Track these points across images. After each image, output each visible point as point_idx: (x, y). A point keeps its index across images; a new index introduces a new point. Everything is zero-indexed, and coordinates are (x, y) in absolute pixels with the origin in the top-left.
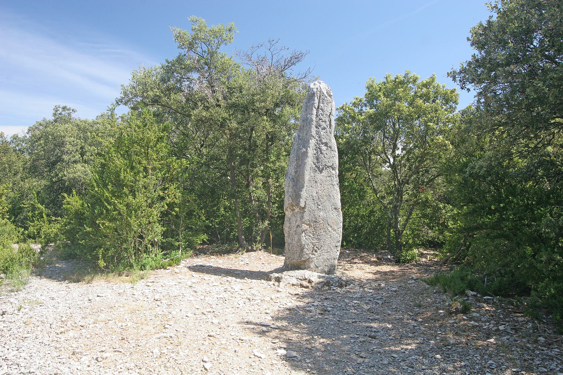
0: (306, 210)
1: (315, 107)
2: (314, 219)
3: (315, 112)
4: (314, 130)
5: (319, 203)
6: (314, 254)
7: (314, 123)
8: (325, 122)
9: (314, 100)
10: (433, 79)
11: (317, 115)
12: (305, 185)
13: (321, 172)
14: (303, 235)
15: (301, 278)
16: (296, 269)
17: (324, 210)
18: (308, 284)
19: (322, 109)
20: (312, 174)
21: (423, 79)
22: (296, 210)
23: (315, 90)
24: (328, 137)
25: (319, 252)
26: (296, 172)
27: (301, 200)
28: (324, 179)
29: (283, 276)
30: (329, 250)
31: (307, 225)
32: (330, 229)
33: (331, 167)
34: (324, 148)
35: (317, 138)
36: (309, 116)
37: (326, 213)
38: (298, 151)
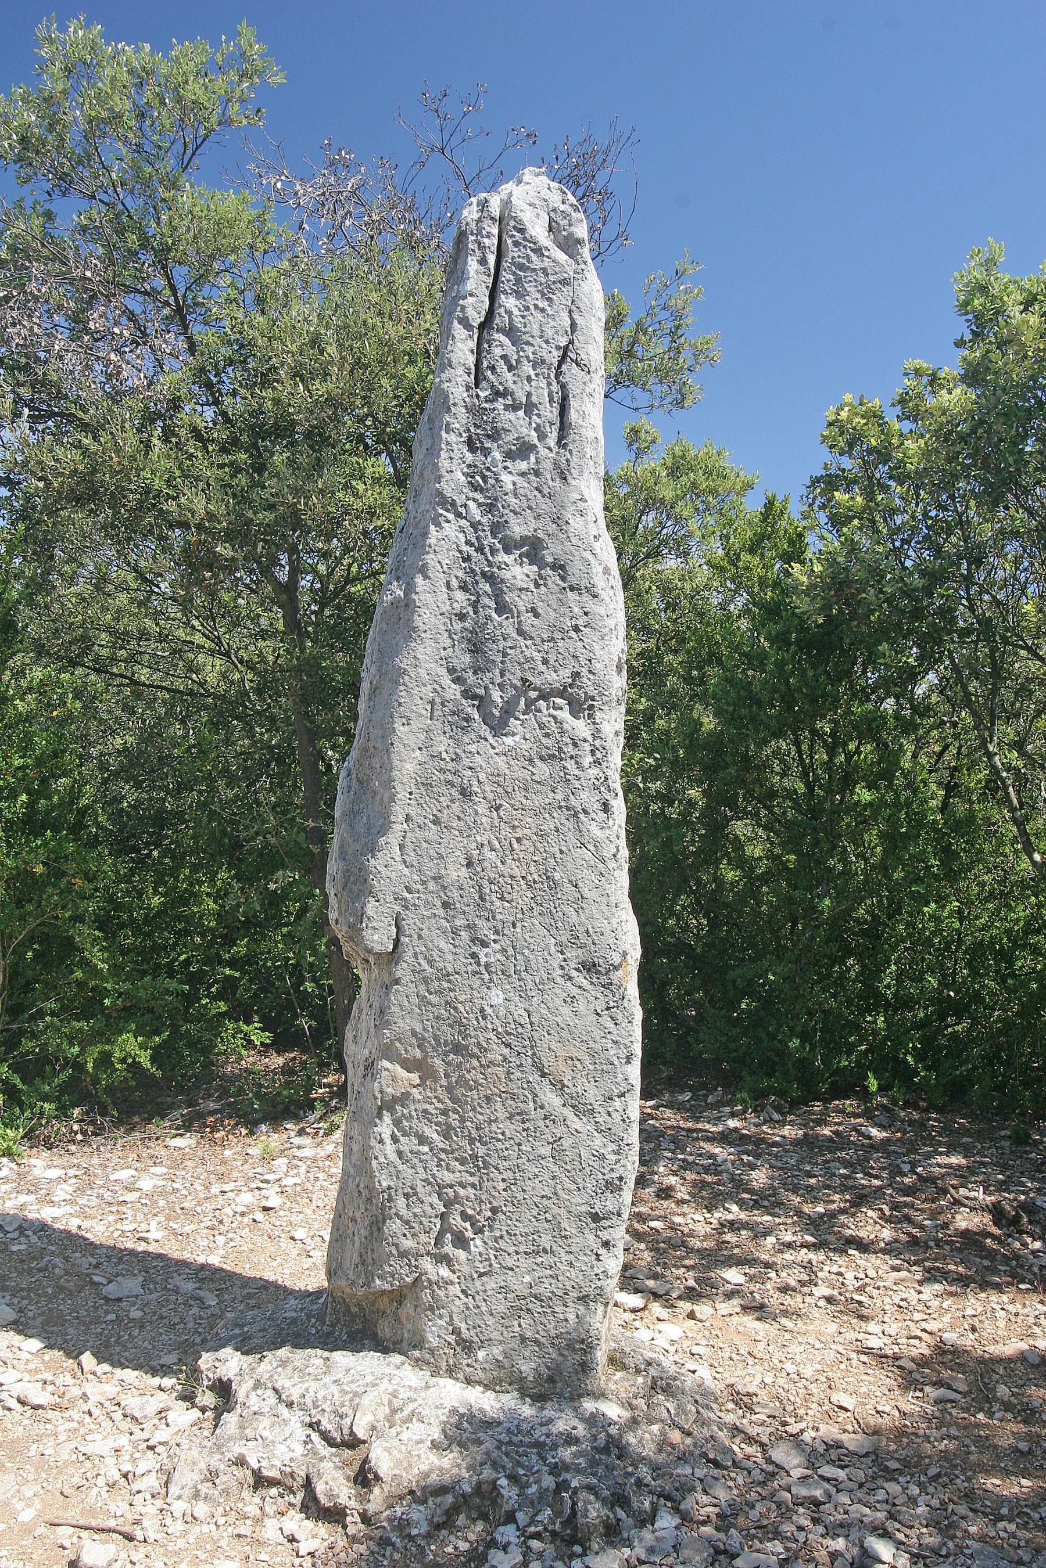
0: (402, 971)
2: (447, 1034)
3: (462, 348)
4: (453, 467)
5: (485, 929)
7: (459, 419)
8: (530, 408)
13: (499, 727)
14: (385, 1128)
16: (329, 1343)
17: (513, 971)
19: (511, 332)
20: (442, 745)
25: (477, 1244)
30: (545, 1241)
31: (409, 1066)
32: (552, 1099)
33: (562, 693)
34: (517, 572)
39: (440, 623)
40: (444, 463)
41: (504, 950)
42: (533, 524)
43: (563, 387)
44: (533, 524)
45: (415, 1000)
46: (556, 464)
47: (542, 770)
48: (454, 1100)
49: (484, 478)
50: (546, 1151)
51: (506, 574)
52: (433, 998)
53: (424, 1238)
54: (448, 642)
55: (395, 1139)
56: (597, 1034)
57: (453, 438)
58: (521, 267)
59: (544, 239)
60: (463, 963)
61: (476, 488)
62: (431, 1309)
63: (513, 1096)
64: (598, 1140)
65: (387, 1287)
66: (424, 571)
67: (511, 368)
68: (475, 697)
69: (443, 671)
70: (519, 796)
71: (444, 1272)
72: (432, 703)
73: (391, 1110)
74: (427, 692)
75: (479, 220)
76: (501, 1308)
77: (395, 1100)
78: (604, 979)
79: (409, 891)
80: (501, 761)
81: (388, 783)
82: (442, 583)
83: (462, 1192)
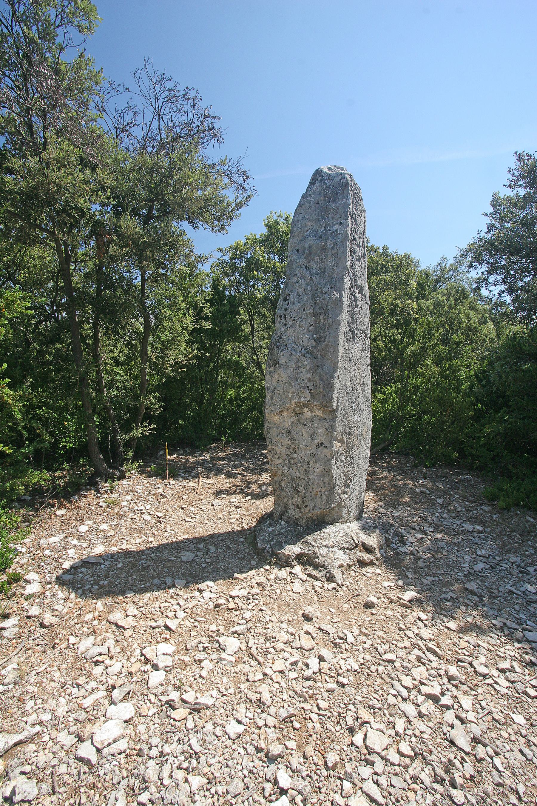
2: (347, 430)
12: (340, 364)
26: (318, 341)
60: (350, 409)
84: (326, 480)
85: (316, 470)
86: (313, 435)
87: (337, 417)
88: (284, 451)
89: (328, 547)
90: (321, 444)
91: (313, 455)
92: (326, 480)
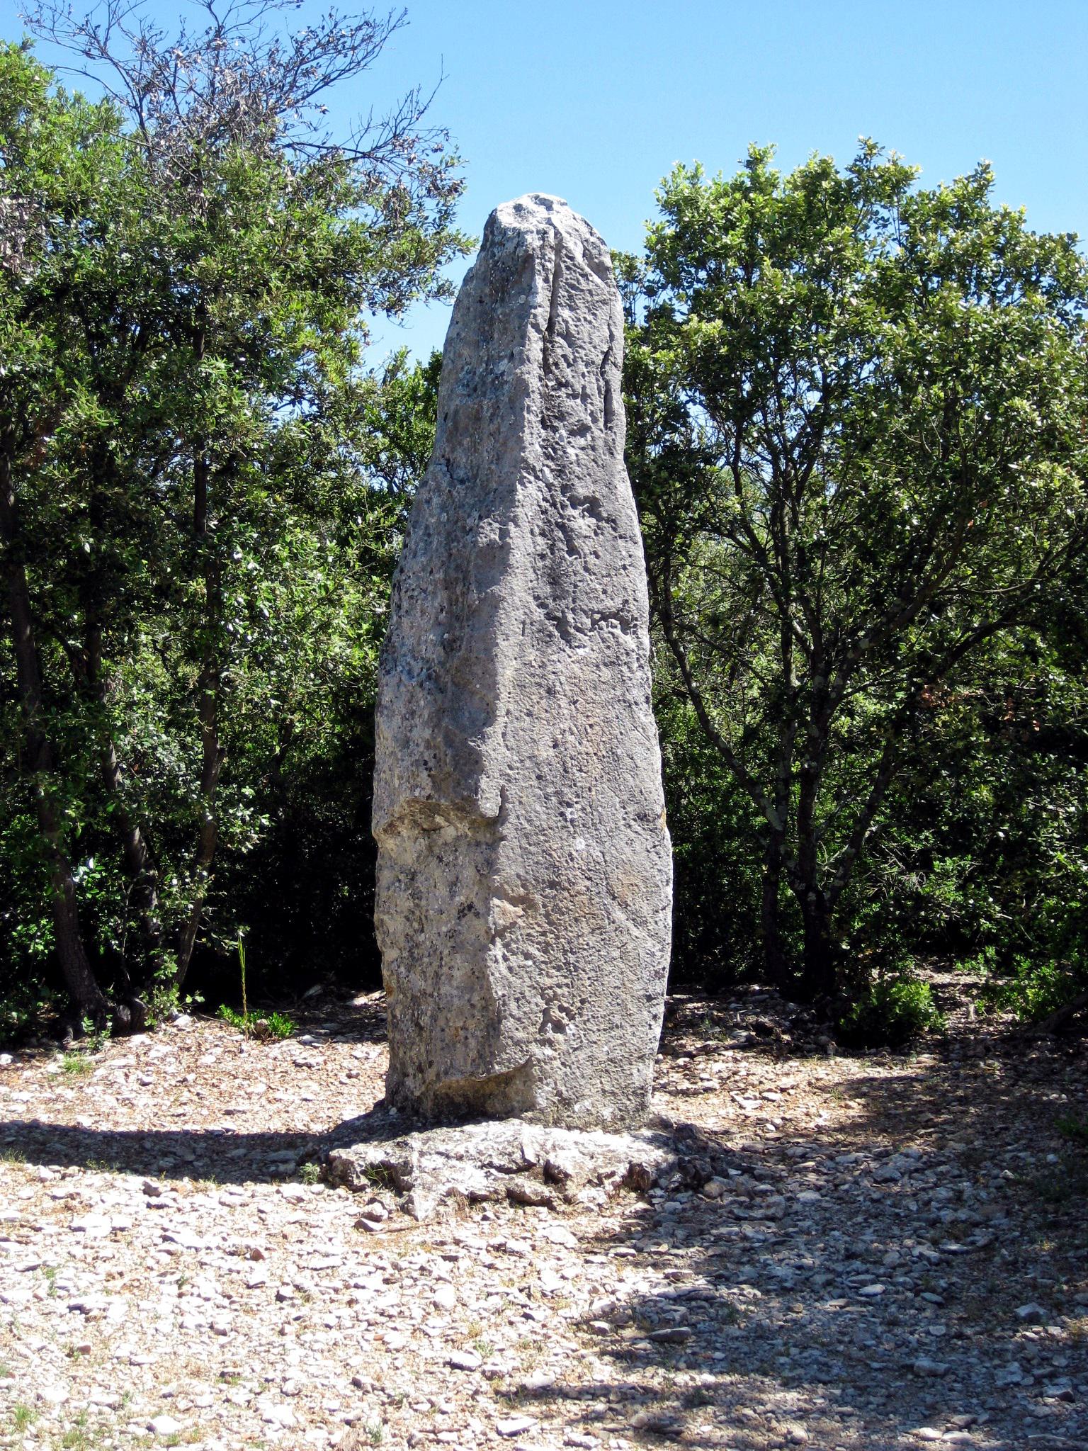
0: (507, 830)
1: (536, 327)
2: (545, 875)
3: (535, 347)
4: (533, 440)
5: (569, 795)
6: (550, 1043)
7: (535, 403)
8: (585, 397)
9: (530, 290)
10: (981, 182)
11: (546, 366)
12: (502, 707)
14: (498, 950)
15: (504, 1161)
17: (591, 824)
18: (547, 1191)
19: (567, 336)
20: (532, 655)
21: (935, 177)
22: (449, 833)
23: (533, 241)
24: (600, 473)
25: (571, 1029)
26: (449, 647)
27: (484, 783)
28: (589, 675)
29: (414, 1158)
30: (617, 1019)
31: (514, 901)
32: (619, 915)
33: (615, 615)
34: (582, 523)
35: (550, 476)
36: (504, 365)
37: (600, 842)
38: (450, 538)
39: (527, 561)
40: (527, 437)
41: (583, 809)
42: (592, 488)
43: (607, 383)
44: (592, 488)
45: (518, 851)
46: (606, 442)
47: (606, 673)
48: (550, 923)
49: (554, 450)
50: (616, 954)
51: (574, 525)
52: (532, 849)
53: (532, 1029)
54: (533, 576)
55: (505, 959)
56: (648, 865)
57: (531, 417)
58: (573, 287)
59: (579, 259)
60: (555, 820)
61: (548, 456)
62: (541, 1080)
63: (594, 916)
64: (650, 943)
65: (504, 1070)
66: (515, 520)
67: (569, 365)
68: (555, 618)
69: (531, 599)
70: (590, 693)
71: (548, 1051)
72: (524, 623)
73: (502, 936)
74: (520, 614)
75: (542, 247)
76: (589, 1072)
77: (505, 928)
78: (651, 826)
79: (511, 768)
80: (576, 667)
81: (492, 686)
82: (527, 530)
83: (559, 991)
84: (476, 999)
85: (456, 973)
86: (453, 884)
87: (503, 838)
88: (400, 927)
89: (448, 1157)
90: (470, 907)
91: (452, 934)
92: (476, 999)
